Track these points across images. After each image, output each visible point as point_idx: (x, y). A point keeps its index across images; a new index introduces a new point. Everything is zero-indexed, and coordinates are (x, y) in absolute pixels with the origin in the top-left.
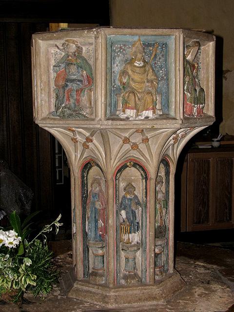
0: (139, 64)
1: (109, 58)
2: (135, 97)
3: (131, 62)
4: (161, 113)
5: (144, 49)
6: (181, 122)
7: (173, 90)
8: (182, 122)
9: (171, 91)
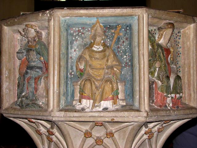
0: (98, 49)
1: (63, 43)
2: (91, 86)
3: (89, 47)
4: (125, 104)
5: (105, 32)
6: (145, 115)
7: (137, 78)
8: (147, 114)
9: (136, 79)
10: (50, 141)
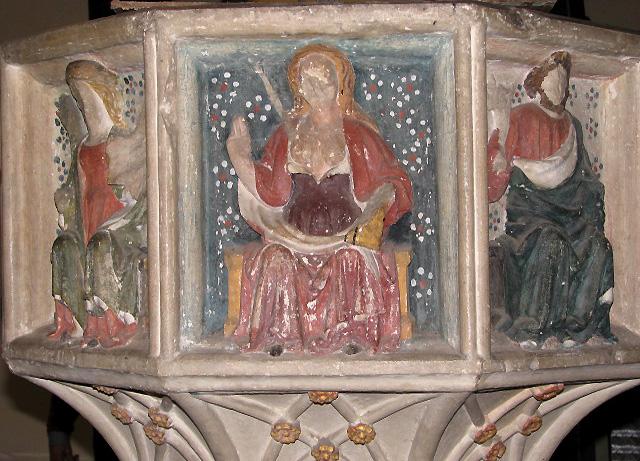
10: (160, 445)
